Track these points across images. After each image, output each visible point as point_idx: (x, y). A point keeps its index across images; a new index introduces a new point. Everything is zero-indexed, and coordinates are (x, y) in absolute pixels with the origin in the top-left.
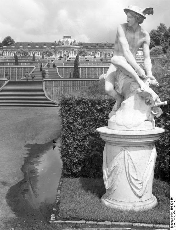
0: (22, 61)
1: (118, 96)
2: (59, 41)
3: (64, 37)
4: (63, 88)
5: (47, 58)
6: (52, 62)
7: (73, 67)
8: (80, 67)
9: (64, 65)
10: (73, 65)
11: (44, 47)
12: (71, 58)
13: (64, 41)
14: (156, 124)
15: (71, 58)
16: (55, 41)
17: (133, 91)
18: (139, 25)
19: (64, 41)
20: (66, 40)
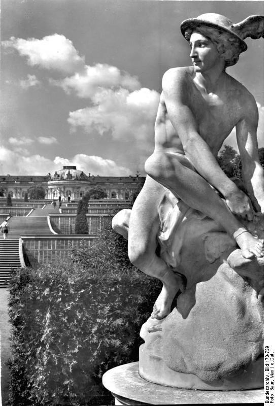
0: (94, 212)
1: (231, 231)
2: (55, 173)
3: (65, 167)
4: (56, 249)
5: (33, 202)
6: (42, 207)
7: (76, 215)
8: (89, 216)
9: (61, 212)
10: (75, 214)
11: (29, 183)
12: (74, 202)
13: (64, 173)
14: (223, 167)
15: (74, 202)
16: (49, 174)
17: (216, 259)
18: (224, 71)
19: (64, 173)
20: (67, 172)
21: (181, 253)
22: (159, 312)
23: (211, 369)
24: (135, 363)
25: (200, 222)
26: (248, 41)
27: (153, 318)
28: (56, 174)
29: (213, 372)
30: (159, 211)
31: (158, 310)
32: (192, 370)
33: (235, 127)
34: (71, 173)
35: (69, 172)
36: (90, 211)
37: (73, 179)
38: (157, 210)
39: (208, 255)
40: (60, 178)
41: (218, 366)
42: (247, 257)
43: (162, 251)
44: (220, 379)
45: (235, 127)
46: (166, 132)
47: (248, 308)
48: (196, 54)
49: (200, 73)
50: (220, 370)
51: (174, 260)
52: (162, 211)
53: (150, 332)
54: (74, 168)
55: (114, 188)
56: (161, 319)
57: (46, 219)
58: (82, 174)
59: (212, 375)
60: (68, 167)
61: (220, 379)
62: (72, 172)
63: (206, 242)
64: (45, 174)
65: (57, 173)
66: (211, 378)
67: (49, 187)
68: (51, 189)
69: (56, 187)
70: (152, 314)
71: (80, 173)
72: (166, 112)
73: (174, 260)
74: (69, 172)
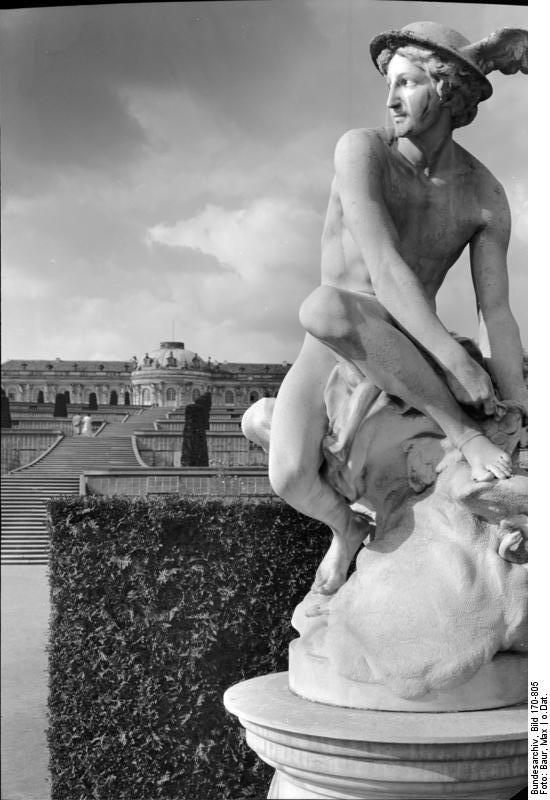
7: (181, 433)
9: (156, 429)
16: (135, 358)
21: (365, 475)
22: (325, 582)
23: (414, 676)
24: (284, 673)
25: (401, 417)
26: (494, 77)
27: (316, 593)
28: (147, 357)
29: (416, 681)
30: (327, 400)
31: (324, 579)
32: (380, 678)
33: (468, 245)
34: (174, 356)
35: (171, 353)
36: (211, 426)
37: (179, 367)
38: (323, 397)
39: (412, 478)
40: (154, 364)
41: (426, 670)
42: (479, 479)
43: (331, 470)
44: (428, 691)
45: (468, 245)
46: (343, 254)
47: (480, 569)
48: (397, 102)
49: (405, 139)
50: (428, 676)
51: (352, 487)
52: (333, 400)
53: (308, 616)
54: (180, 346)
55: (254, 386)
56: (331, 592)
57: (130, 439)
58: (196, 359)
59: (415, 686)
60: (324, 738)
61: (428, 691)
62: (177, 354)
63: (410, 455)
64: (127, 358)
65: (150, 356)
66: (414, 692)
67: (135, 382)
68: (139, 386)
69: (147, 381)
70: (314, 586)
71: (192, 358)
72: (341, 214)
73: (352, 487)
74: (171, 353)
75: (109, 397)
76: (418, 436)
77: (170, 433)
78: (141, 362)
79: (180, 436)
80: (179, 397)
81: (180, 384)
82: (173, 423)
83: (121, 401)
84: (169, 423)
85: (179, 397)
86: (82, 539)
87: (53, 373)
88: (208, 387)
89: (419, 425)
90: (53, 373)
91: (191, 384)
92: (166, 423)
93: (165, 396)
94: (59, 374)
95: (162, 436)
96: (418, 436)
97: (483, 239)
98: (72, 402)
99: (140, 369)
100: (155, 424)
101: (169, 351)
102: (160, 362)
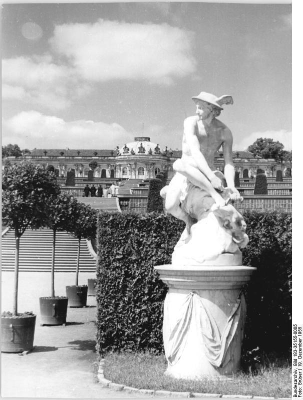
9: (131, 194)
16: (118, 147)
28: (126, 147)
34: (143, 146)
36: (241, 185)
51: (188, 209)
62: (146, 145)
64: (113, 148)
65: (127, 146)
73: (188, 209)
75: (101, 173)
76: (205, 196)
77: (140, 196)
78: (121, 151)
79: (146, 198)
80: (146, 172)
81: (147, 164)
82: (142, 190)
83: (108, 175)
84: (140, 190)
85: (146, 172)
86: (147, 163)
87: (64, 157)
88: (166, 166)
89: (205, 194)
90: (64, 157)
91: (154, 164)
92: (138, 190)
93: (137, 172)
94: (67, 158)
95: (135, 198)
96: (205, 196)
97: (224, 144)
98: (76, 176)
99: (120, 155)
100: (131, 191)
101: (140, 143)
102: (134, 150)
